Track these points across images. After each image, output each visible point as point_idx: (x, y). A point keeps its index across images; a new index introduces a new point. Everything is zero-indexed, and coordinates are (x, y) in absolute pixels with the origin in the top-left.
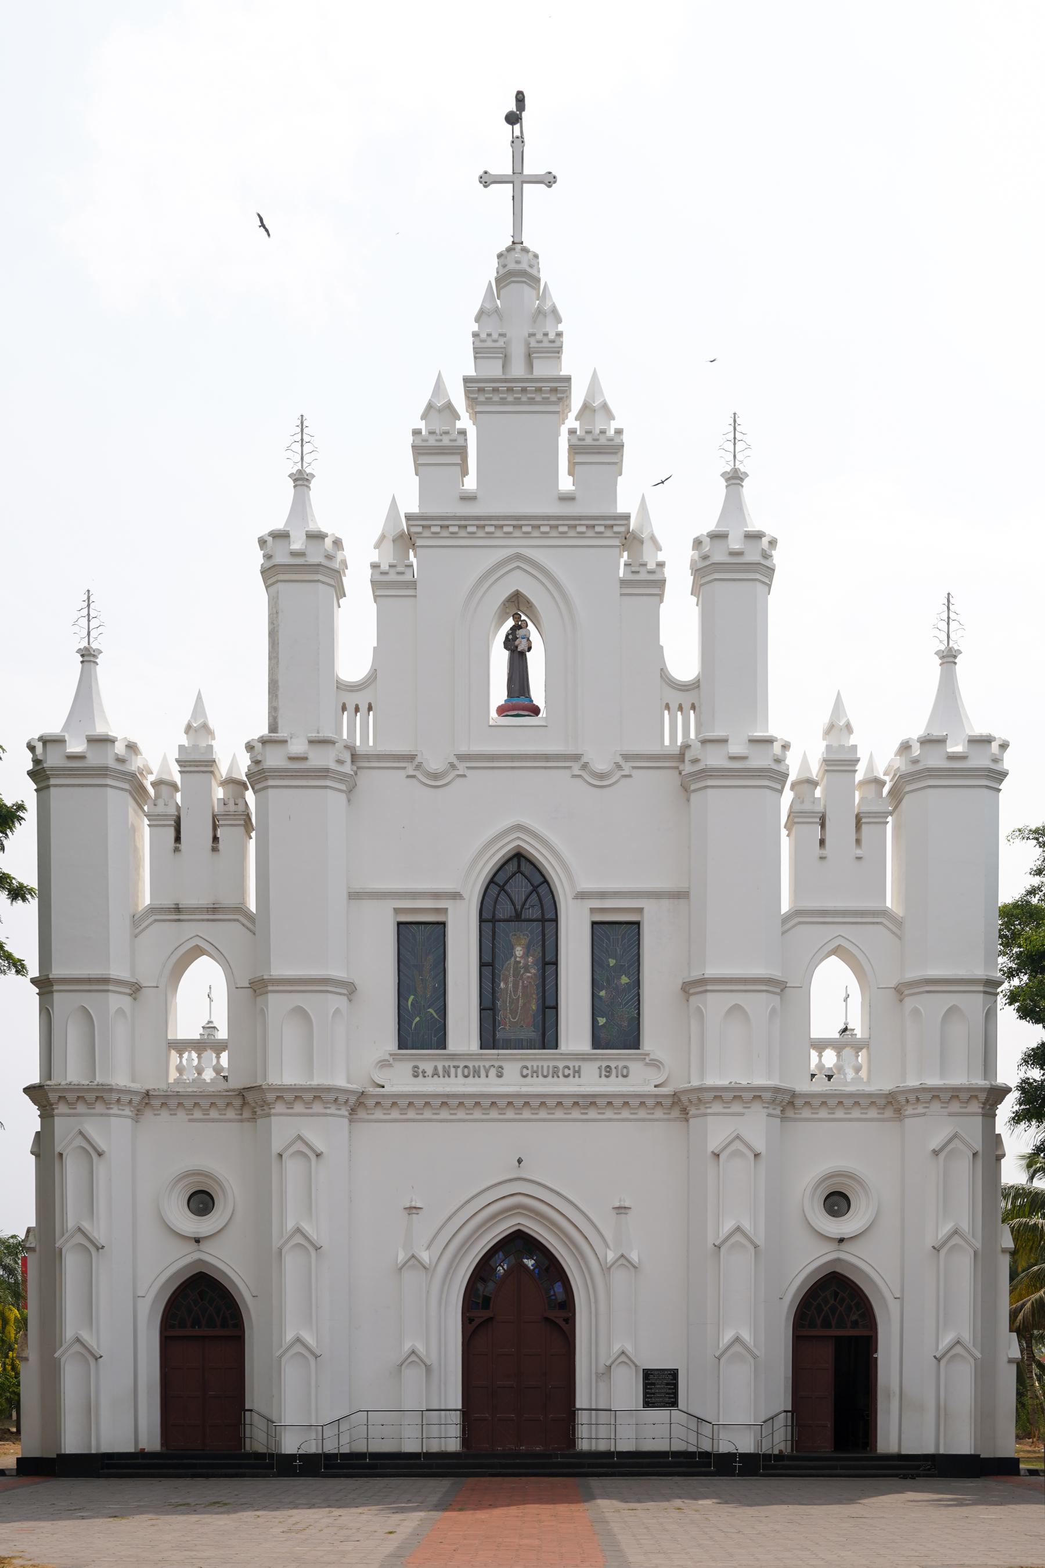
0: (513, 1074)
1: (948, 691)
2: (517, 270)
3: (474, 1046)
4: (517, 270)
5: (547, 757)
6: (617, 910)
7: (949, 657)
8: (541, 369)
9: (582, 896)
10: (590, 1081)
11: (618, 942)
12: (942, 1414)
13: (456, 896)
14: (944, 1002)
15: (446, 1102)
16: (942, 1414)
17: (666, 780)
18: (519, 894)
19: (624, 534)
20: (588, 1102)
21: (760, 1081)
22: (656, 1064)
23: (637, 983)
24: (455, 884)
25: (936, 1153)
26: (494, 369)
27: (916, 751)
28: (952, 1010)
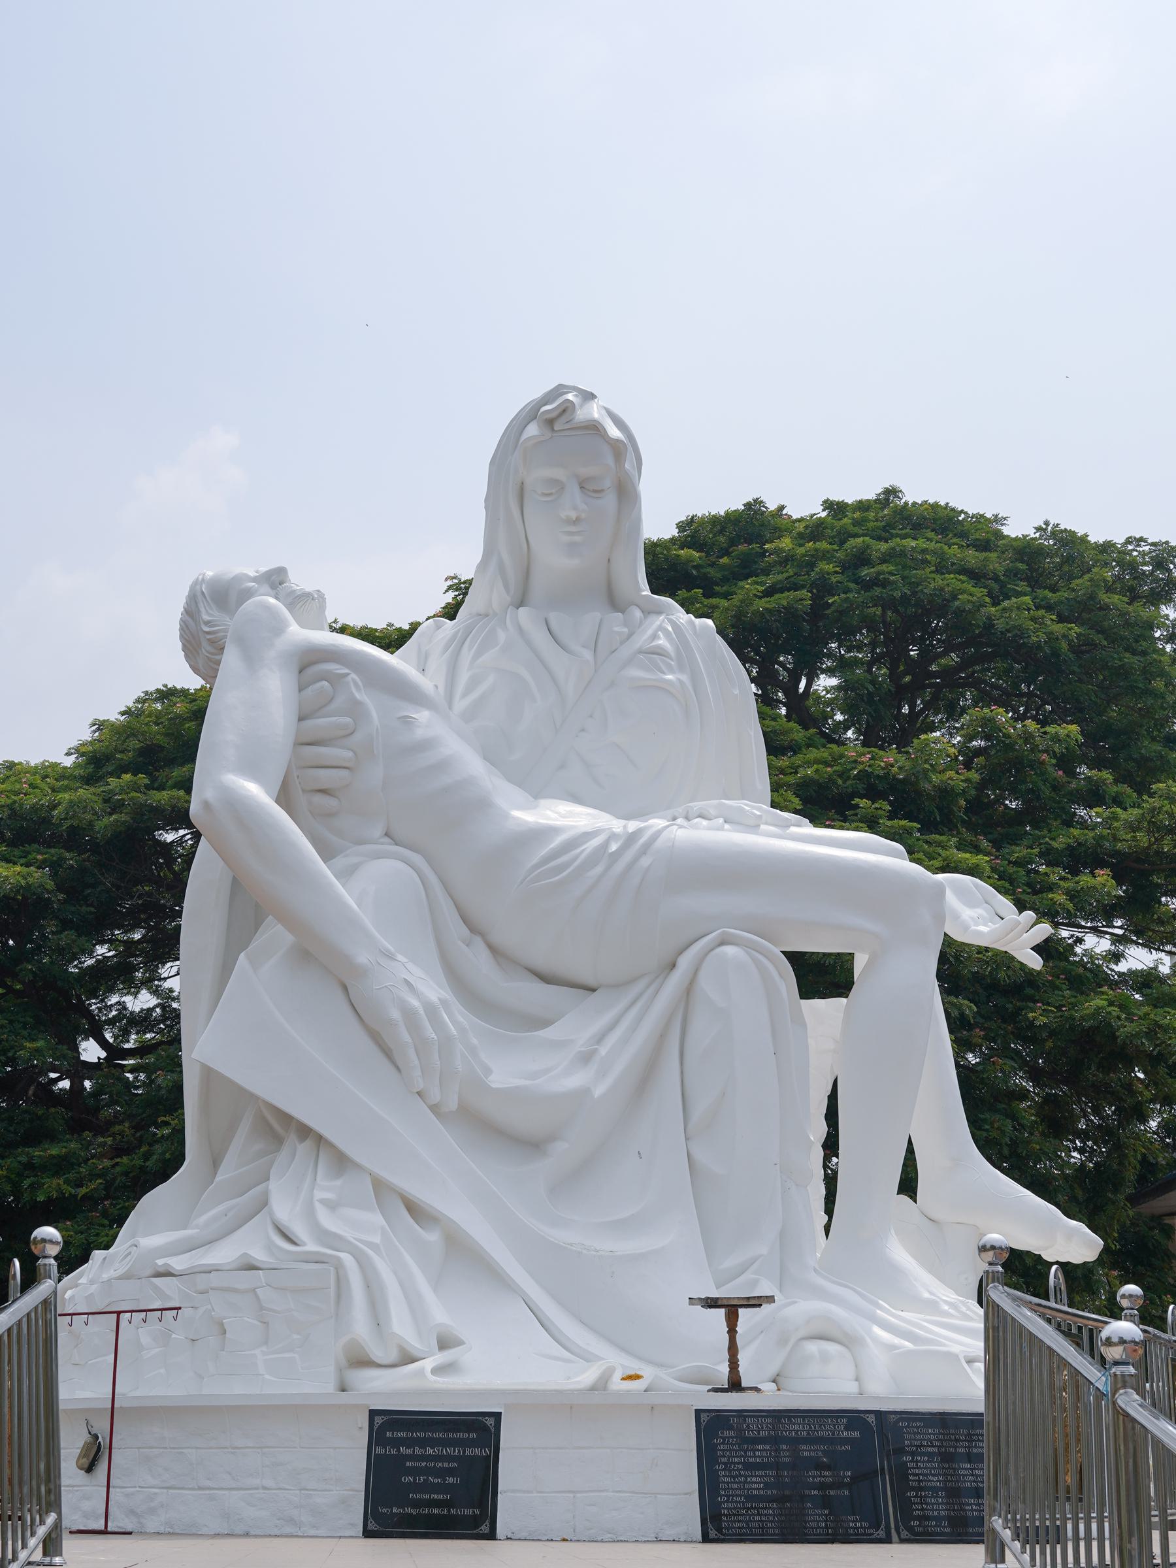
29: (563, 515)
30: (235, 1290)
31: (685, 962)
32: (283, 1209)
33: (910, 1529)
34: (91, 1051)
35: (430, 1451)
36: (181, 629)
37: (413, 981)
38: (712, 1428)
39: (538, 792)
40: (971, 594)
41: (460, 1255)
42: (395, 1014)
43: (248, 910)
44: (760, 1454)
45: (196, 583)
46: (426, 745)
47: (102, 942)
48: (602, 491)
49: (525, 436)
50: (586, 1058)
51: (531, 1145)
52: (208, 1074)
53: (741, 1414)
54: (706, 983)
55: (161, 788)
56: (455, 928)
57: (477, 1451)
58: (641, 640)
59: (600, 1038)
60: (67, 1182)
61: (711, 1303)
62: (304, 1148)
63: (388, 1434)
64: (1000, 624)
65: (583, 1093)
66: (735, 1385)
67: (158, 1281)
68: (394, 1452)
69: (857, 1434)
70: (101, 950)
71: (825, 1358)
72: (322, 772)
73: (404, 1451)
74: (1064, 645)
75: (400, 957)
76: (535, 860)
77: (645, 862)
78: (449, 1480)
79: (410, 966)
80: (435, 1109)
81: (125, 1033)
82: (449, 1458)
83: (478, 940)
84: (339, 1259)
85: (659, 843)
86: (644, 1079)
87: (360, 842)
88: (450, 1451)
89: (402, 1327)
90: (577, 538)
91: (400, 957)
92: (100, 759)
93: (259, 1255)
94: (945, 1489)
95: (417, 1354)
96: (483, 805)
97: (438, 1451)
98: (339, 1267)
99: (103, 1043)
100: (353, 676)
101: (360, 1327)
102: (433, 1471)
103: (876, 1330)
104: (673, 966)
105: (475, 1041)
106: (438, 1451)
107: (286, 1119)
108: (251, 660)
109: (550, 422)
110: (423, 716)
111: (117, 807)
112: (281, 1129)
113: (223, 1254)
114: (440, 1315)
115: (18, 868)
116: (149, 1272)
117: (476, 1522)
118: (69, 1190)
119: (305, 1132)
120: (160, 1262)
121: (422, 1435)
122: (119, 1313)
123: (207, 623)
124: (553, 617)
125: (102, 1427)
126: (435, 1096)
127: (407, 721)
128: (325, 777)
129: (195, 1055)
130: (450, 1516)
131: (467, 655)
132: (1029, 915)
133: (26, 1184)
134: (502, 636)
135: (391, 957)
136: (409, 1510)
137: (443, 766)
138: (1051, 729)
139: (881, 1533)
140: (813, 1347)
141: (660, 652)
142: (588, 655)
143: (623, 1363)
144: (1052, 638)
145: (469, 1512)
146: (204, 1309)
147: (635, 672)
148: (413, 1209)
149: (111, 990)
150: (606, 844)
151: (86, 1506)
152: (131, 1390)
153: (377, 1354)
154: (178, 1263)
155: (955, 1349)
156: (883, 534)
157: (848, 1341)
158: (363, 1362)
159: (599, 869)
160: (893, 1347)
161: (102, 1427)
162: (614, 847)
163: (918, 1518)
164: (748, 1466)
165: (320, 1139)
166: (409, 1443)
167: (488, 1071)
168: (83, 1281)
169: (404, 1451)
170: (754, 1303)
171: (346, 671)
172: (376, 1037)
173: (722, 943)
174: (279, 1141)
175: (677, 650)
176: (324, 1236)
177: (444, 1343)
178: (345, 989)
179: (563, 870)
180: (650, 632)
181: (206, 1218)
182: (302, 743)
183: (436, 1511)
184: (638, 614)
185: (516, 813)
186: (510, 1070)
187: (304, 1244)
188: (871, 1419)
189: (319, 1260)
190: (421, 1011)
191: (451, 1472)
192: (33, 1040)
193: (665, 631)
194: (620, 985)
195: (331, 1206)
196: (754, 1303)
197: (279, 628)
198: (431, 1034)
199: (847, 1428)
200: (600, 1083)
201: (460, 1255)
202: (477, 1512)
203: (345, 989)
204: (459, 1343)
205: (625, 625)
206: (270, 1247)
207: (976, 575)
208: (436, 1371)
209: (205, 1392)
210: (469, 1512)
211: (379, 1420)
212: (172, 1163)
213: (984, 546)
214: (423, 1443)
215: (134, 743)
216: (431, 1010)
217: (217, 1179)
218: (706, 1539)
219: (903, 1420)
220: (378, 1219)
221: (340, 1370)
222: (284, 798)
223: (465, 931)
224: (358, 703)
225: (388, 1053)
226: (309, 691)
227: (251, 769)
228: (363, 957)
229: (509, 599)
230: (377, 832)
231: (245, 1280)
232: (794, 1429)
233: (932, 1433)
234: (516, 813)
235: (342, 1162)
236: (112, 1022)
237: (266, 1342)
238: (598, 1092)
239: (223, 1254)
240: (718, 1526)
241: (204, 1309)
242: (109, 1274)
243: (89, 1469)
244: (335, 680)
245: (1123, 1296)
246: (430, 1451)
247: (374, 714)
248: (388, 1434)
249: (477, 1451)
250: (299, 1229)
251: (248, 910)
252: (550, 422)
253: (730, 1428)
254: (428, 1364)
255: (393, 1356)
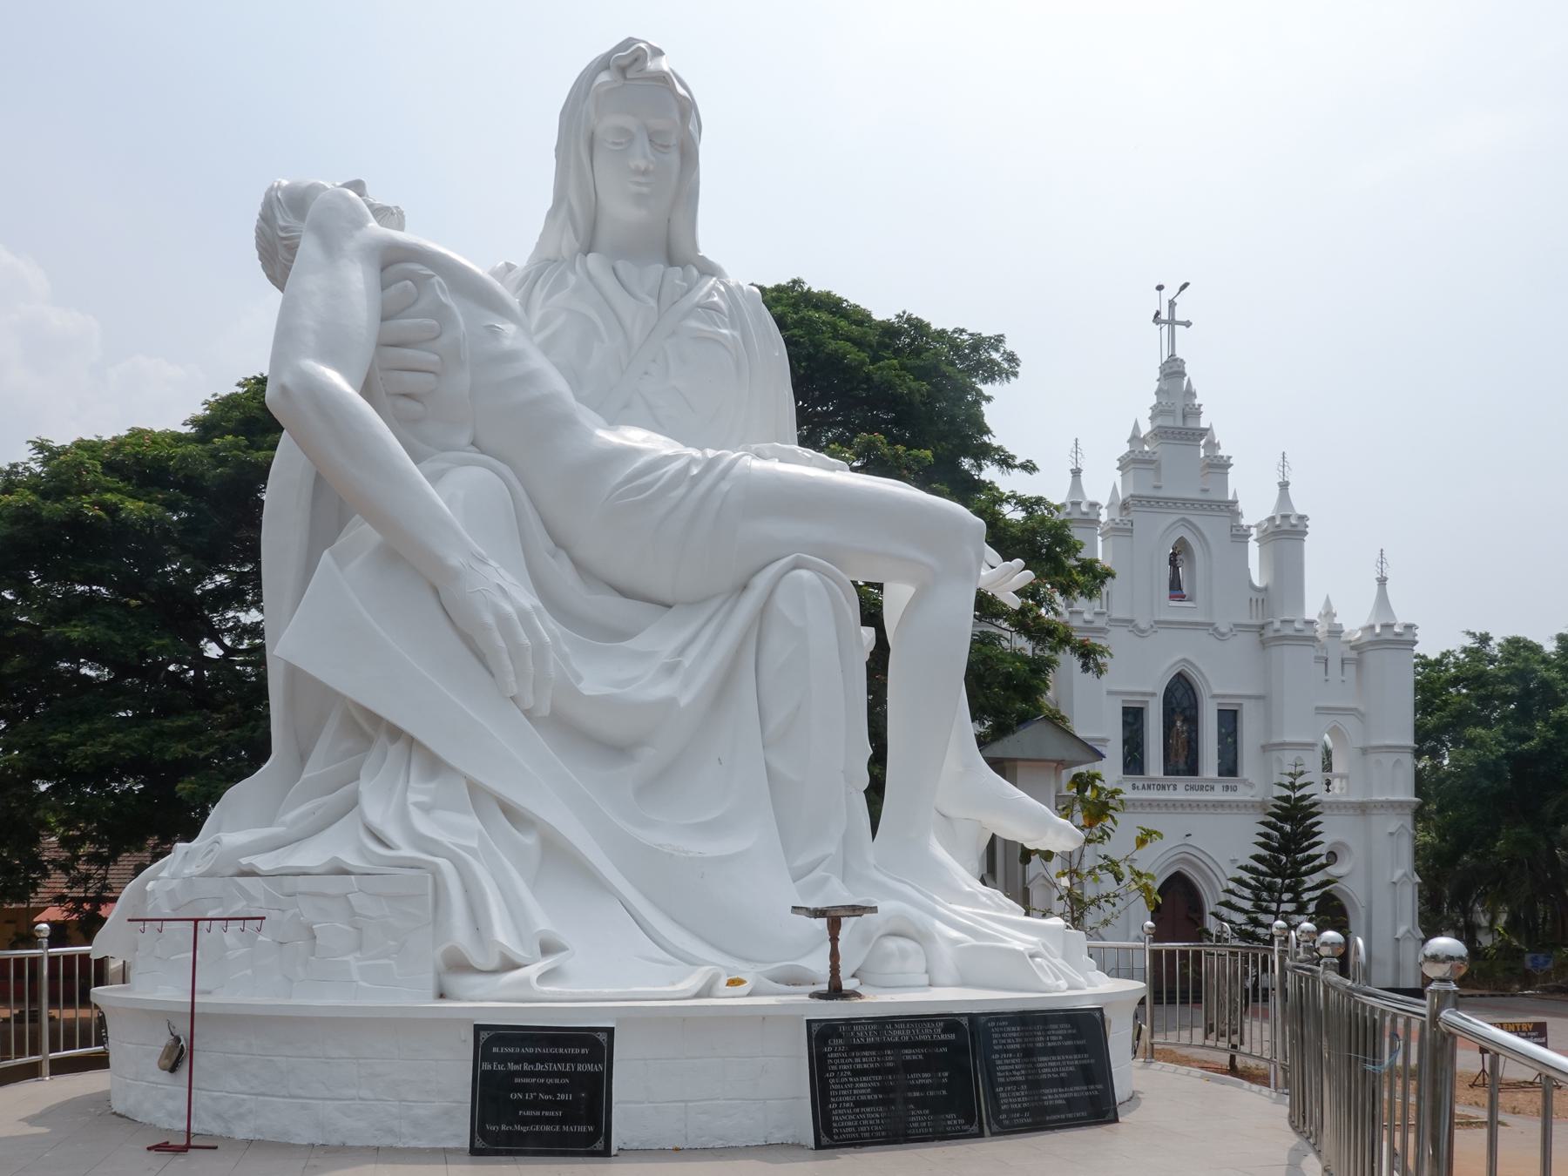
0: (1180, 790)
1: (1383, 600)
2: (1173, 370)
3: (1215, 775)
4: (1173, 370)
5: (1197, 624)
6: (1230, 704)
7: (1382, 581)
8: (1191, 424)
9: (1214, 696)
10: (1218, 795)
11: (1229, 720)
12: (1398, 966)
13: (1153, 694)
14: (1395, 757)
15: (1151, 804)
16: (1398, 966)
17: (1250, 639)
18: (1181, 698)
19: (1230, 509)
20: (1219, 805)
21: (1353, 799)
22: (1251, 786)
23: (1235, 742)
24: (1150, 686)
25: (1391, 834)
26: (1168, 422)
27: (1378, 630)
28: (1398, 761)
29: (632, 164)
30: (324, 895)
31: (761, 583)
32: (375, 810)
33: (999, 1123)
34: (213, 651)
35: (539, 1067)
36: (258, 237)
37: (503, 585)
38: (822, 1036)
39: (613, 422)
40: (854, 355)
41: (557, 857)
42: (489, 619)
43: (332, 508)
44: (867, 1060)
45: (272, 188)
46: (511, 356)
47: (221, 571)
48: (667, 147)
49: (597, 82)
50: (671, 669)
51: (616, 750)
52: (293, 672)
53: (849, 1022)
54: (782, 603)
55: (259, 449)
56: (542, 541)
57: (590, 1067)
58: (699, 295)
59: (682, 651)
60: (190, 747)
61: (818, 913)
62: (395, 750)
63: (495, 1050)
64: (876, 377)
65: (670, 702)
66: (836, 991)
67: (241, 880)
68: (501, 1068)
69: (953, 1036)
70: (220, 578)
71: (904, 955)
72: (406, 375)
73: (512, 1067)
74: (918, 396)
75: (492, 562)
76: (620, 478)
77: (725, 486)
78: (562, 1097)
79: (502, 571)
80: (528, 713)
81: (240, 639)
82: (560, 1074)
83: (563, 554)
84: (436, 865)
85: (736, 470)
86: (723, 689)
87: (447, 448)
88: (561, 1067)
89: (503, 934)
90: (645, 190)
91: (492, 562)
92: (207, 428)
93: (351, 859)
94: (1026, 1082)
95: (519, 960)
96: (568, 421)
97: (549, 1067)
98: (436, 872)
99: (222, 645)
100: (438, 278)
101: (460, 935)
102: (544, 1084)
103: (939, 925)
104: (744, 587)
105: (566, 649)
106: (549, 1067)
107: (375, 719)
108: (330, 246)
109: (623, 70)
110: (509, 328)
111: (223, 462)
112: (371, 731)
113: (310, 856)
114: (543, 923)
115: (142, 504)
116: (232, 870)
117: (591, 1138)
118: (191, 752)
119: (396, 733)
120: (244, 861)
121: (531, 1050)
122: (196, 921)
123: (284, 229)
124: (620, 265)
125: (183, 1029)
126: (529, 701)
127: (494, 332)
128: (411, 381)
129: (276, 653)
130: (561, 1133)
131: (539, 294)
132: (1019, 562)
133: (156, 746)
134: (572, 279)
135: (483, 561)
136: (518, 1128)
137: (530, 378)
138: (915, 452)
139: (975, 1128)
140: (893, 944)
141: (714, 308)
142: (652, 303)
143: (717, 964)
144: (911, 392)
145: (582, 1129)
146: (291, 912)
147: (693, 323)
148: (510, 812)
149: (228, 608)
150: (687, 468)
151: (170, 1105)
152: (219, 994)
153: (477, 960)
154: (263, 862)
155: (1019, 946)
156: (795, 306)
157: (921, 937)
158: (459, 965)
159: (681, 491)
160: (956, 942)
161: (183, 1029)
162: (695, 471)
163: (1006, 1111)
164: (857, 1073)
165: (412, 741)
166: (518, 1059)
167: (579, 678)
168: (164, 874)
169: (512, 1067)
170: (856, 910)
171: (430, 272)
172: (468, 640)
173: (795, 567)
174: (368, 741)
175: (730, 309)
176: (419, 841)
177: (547, 948)
178: (436, 592)
179: (645, 489)
180: (706, 289)
181: (293, 816)
182: (384, 344)
183: (547, 1128)
184: (695, 272)
185: (600, 433)
186: (598, 677)
187: (398, 848)
188: (965, 1021)
189: (414, 865)
190: (515, 617)
191: (561, 1088)
192: (159, 638)
193: (718, 290)
194: (695, 603)
195: (426, 809)
196: (856, 910)
197: (359, 223)
198: (525, 639)
199: (944, 1031)
200: (686, 692)
201: (557, 857)
202: (591, 1129)
203: (436, 592)
204: (563, 949)
205: (684, 280)
206: (362, 851)
207: (859, 343)
208: (545, 977)
209: (296, 1001)
210: (582, 1129)
211: (484, 1035)
212: (260, 752)
213: (860, 323)
214: (532, 1059)
215: (236, 414)
216: (524, 616)
217: (305, 776)
218: (819, 1145)
219: (990, 1020)
220: (473, 822)
221: (438, 974)
222: (367, 391)
223: (552, 544)
224: (445, 307)
225: (481, 657)
226: (393, 290)
227: (331, 356)
228: (455, 560)
229: (577, 245)
230: (464, 439)
231: (335, 885)
232: (896, 1035)
233: (1014, 1031)
234: (600, 433)
235: (435, 766)
236: (230, 630)
237: (360, 948)
238: (684, 701)
239: (310, 856)
240: (831, 1134)
241: (291, 912)
242: (191, 870)
243: (173, 1069)
244: (420, 281)
245: (1325, 944)
246: (539, 1067)
247: (461, 319)
248: (495, 1050)
249: (590, 1067)
250: (392, 832)
251: (332, 508)
252: (623, 70)
253: (840, 1036)
254: (532, 972)
255: (494, 963)
